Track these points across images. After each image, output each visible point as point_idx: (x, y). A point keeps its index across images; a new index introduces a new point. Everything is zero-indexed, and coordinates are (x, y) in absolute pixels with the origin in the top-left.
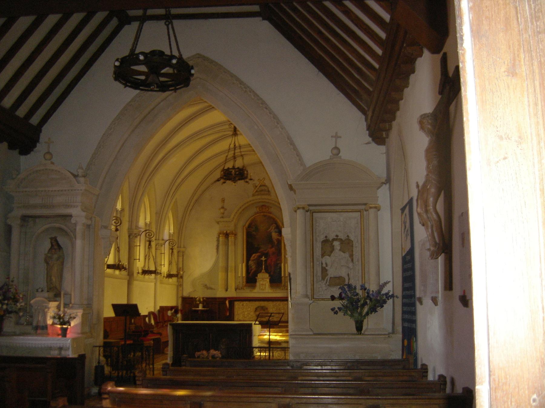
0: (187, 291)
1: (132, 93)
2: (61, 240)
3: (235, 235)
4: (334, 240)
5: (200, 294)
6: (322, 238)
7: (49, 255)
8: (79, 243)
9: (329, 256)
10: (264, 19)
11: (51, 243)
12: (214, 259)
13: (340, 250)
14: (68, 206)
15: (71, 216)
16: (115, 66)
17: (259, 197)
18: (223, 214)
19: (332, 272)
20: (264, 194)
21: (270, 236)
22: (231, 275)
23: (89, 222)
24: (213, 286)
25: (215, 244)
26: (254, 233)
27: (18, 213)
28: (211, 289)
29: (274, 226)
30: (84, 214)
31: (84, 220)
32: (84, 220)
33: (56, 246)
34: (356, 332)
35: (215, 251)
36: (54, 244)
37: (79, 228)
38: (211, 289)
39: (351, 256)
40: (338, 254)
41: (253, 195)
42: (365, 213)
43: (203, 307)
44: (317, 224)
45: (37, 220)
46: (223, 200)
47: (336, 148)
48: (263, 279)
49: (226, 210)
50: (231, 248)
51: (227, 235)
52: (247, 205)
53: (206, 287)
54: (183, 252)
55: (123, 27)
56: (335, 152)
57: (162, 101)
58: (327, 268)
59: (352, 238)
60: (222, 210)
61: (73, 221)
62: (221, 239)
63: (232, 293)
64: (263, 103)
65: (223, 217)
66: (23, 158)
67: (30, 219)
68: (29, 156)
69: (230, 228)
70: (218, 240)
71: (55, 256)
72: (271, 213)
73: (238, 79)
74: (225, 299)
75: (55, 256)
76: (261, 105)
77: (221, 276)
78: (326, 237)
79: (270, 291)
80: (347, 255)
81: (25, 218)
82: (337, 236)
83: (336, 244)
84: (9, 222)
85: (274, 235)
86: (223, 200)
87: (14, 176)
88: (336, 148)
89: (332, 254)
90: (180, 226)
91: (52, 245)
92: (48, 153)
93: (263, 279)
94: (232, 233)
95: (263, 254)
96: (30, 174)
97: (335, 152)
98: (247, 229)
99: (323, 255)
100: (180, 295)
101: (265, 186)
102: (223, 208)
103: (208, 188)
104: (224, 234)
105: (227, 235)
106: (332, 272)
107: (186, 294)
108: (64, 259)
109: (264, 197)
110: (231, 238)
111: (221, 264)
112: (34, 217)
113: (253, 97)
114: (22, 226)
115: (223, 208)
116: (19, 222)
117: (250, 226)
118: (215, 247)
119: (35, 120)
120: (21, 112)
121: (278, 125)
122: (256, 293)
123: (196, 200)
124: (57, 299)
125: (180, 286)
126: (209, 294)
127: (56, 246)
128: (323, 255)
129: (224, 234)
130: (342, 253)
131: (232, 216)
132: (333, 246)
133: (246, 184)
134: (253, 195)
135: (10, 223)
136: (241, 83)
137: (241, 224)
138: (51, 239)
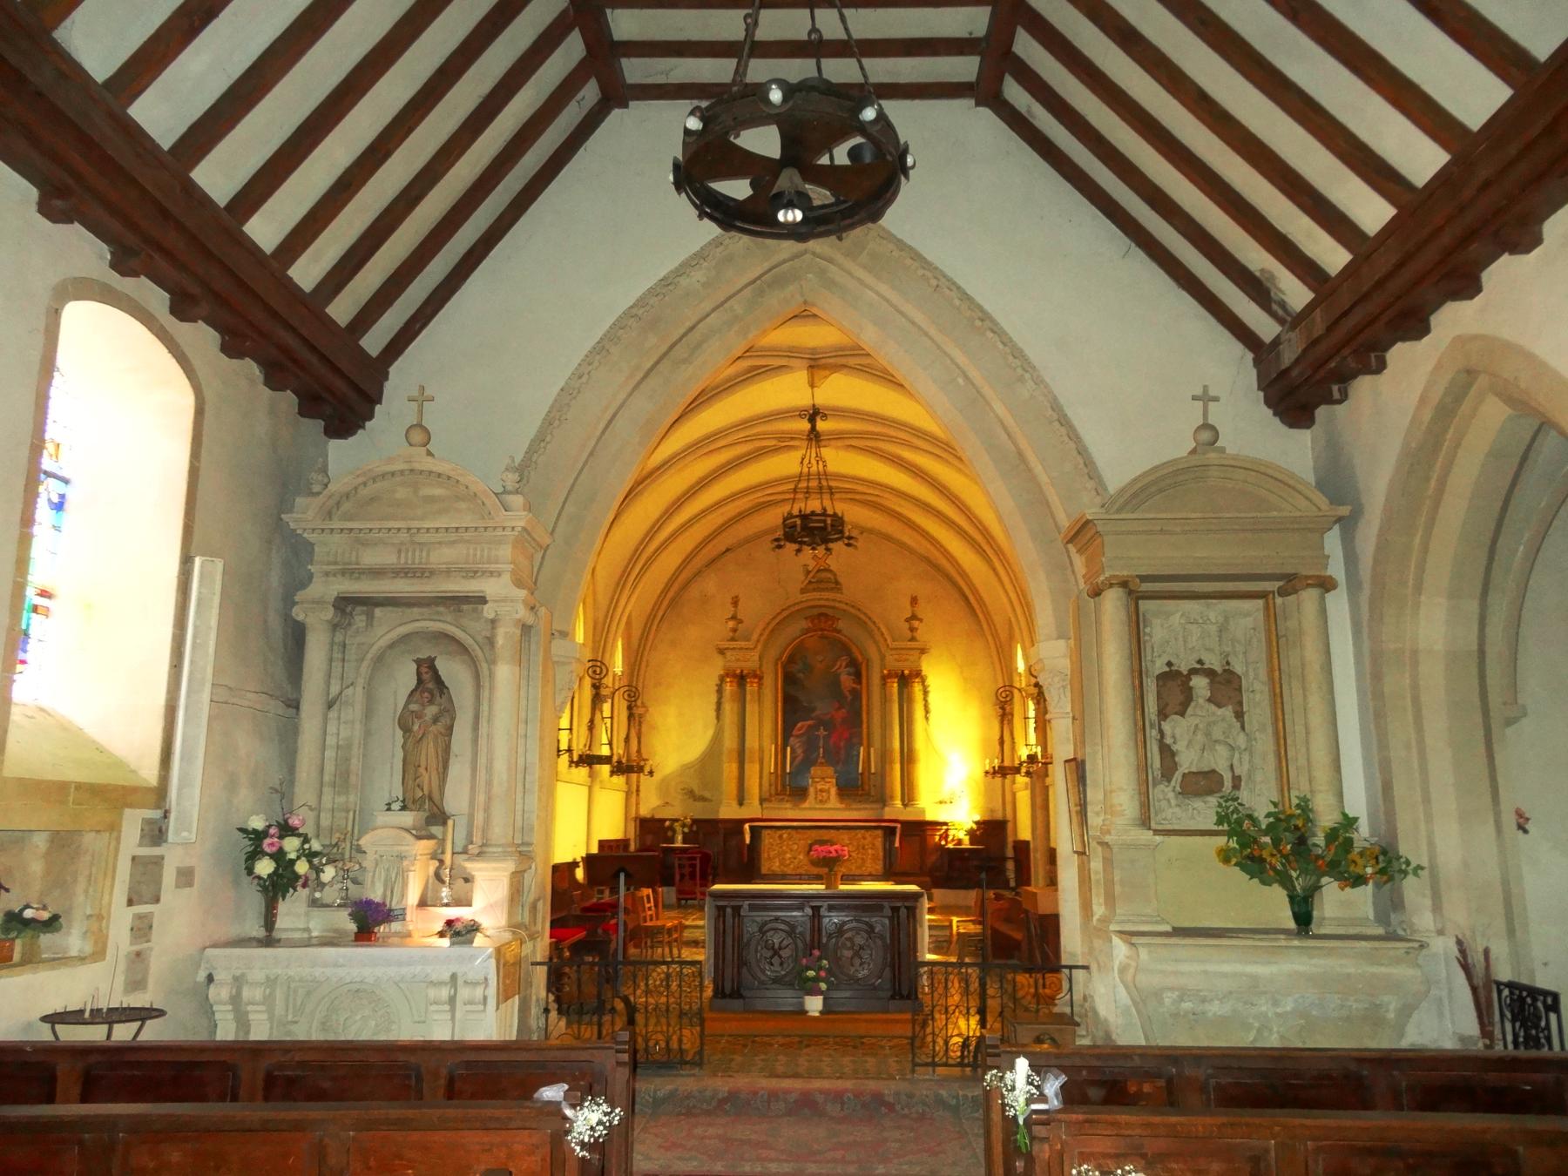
0: (650, 804)
1: (710, 229)
2: (452, 670)
3: (761, 678)
4: (1193, 671)
5: (678, 810)
6: (1159, 667)
7: (414, 707)
8: (505, 673)
9: (1182, 714)
10: (978, 104)
11: (419, 674)
12: (710, 733)
13: (1209, 700)
14: (474, 574)
15: (482, 600)
16: (687, 132)
17: (816, 595)
18: (734, 630)
19: (1188, 760)
20: (826, 589)
21: (835, 683)
22: (752, 771)
23: (530, 620)
24: (707, 795)
25: (714, 698)
26: (801, 675)
27: (325, 588)
28: (703, 799)
29: (843, 661)
30: (523, 593)
31: (522, 613)
32: (522, 613)
33: (430, 683)
34: (1292, 925)
35: (714, 714)
36: (426, 677)
37: (505, 636)
38: (703, 799)
39: (1239, 715)
40: (1202, 710)
41: (803, 591)
42: (1279, 600)
43: (684, 842)
44: (1148, 630)
45: (378, 612)
46: (735, 602)
47: (1206, 426)
48: (823, 782)
49: (741, 621)
50: (751, 709)
51: (741, 679)
52: (785, 614)
53: (691, 794)
54: (641, 716)
55: (608, 113)
56: (1206, 436)
57: (714, 310)
58: (1174, 748)
59: (1238, 668)
60: (731, 624)
61: (488, 611)
62: (728, 688)
63: (753, 809)
64: (985, 316)
65: (733, 639)
66: (335, 445)
67: (359, 609)
68: (351, 440)
69: (751, 661)
70: (720, 691)
71: (431, 710)
72: (839, 632)
73: (916, 256)
74: (740, 823)
75: (431, 710)
76: (978, 323)
77: (730, 769)
78: (1169, 664)
79: (839, 806)
80: (1227, 712)
81: (345, 604)
82: (1200, 662)
83: (1200, 684)
84: (298, 614)
85: (846, 681)
86: (735, 602)
87: (316, 488)
88: (1206, 426)
89: (1190, 711)
90: (635, 661)
91: (420, 681)
92: (420, 426)
93: (823, 782)
94: (755, 676)
95: (821, 722)
96: (365, 484)
97: (1206, 436)
98: (784, 667)
99: (1163, 714)
100: (633, 815)
101: (828, 570)
102: (734, 618)
103: (698, 573)
104: (734, 676)
105: (741, 679)
106: (1188, 760)
107: (645, 811)
108: (453, 719)
109: (826, 595)
110: (751, 688)
111: (730, 741)
112: (369, 603)
113: (957, 302)
114: (335, 627)
115: (734, 618)
116: (329, 613)
117: (791, 660)
118: (714, 707)
119: (373, 342)
120: (342, 310)
121: (1027, 376)
122: (809, 810)
123: (673, 600)
124: (436, 830)
125: (632, 794)
126: (700, 811)
127: (430, 683)
128: (1163, 714)
129: (734, 676)
130: (1213, 707)
131: (755, 637)
132: (1191, 689)
133: (850, 549)
134: (803, 591)
135: (300, 618)
136: (926, 264)
137: (773, 653)
138: (419, 662)
